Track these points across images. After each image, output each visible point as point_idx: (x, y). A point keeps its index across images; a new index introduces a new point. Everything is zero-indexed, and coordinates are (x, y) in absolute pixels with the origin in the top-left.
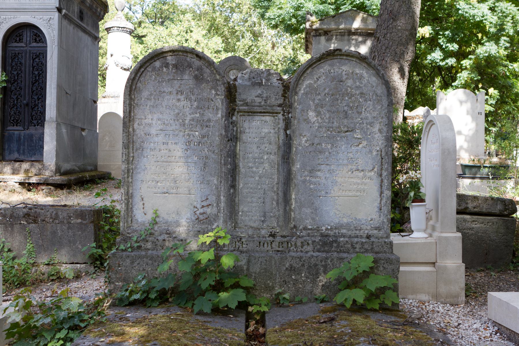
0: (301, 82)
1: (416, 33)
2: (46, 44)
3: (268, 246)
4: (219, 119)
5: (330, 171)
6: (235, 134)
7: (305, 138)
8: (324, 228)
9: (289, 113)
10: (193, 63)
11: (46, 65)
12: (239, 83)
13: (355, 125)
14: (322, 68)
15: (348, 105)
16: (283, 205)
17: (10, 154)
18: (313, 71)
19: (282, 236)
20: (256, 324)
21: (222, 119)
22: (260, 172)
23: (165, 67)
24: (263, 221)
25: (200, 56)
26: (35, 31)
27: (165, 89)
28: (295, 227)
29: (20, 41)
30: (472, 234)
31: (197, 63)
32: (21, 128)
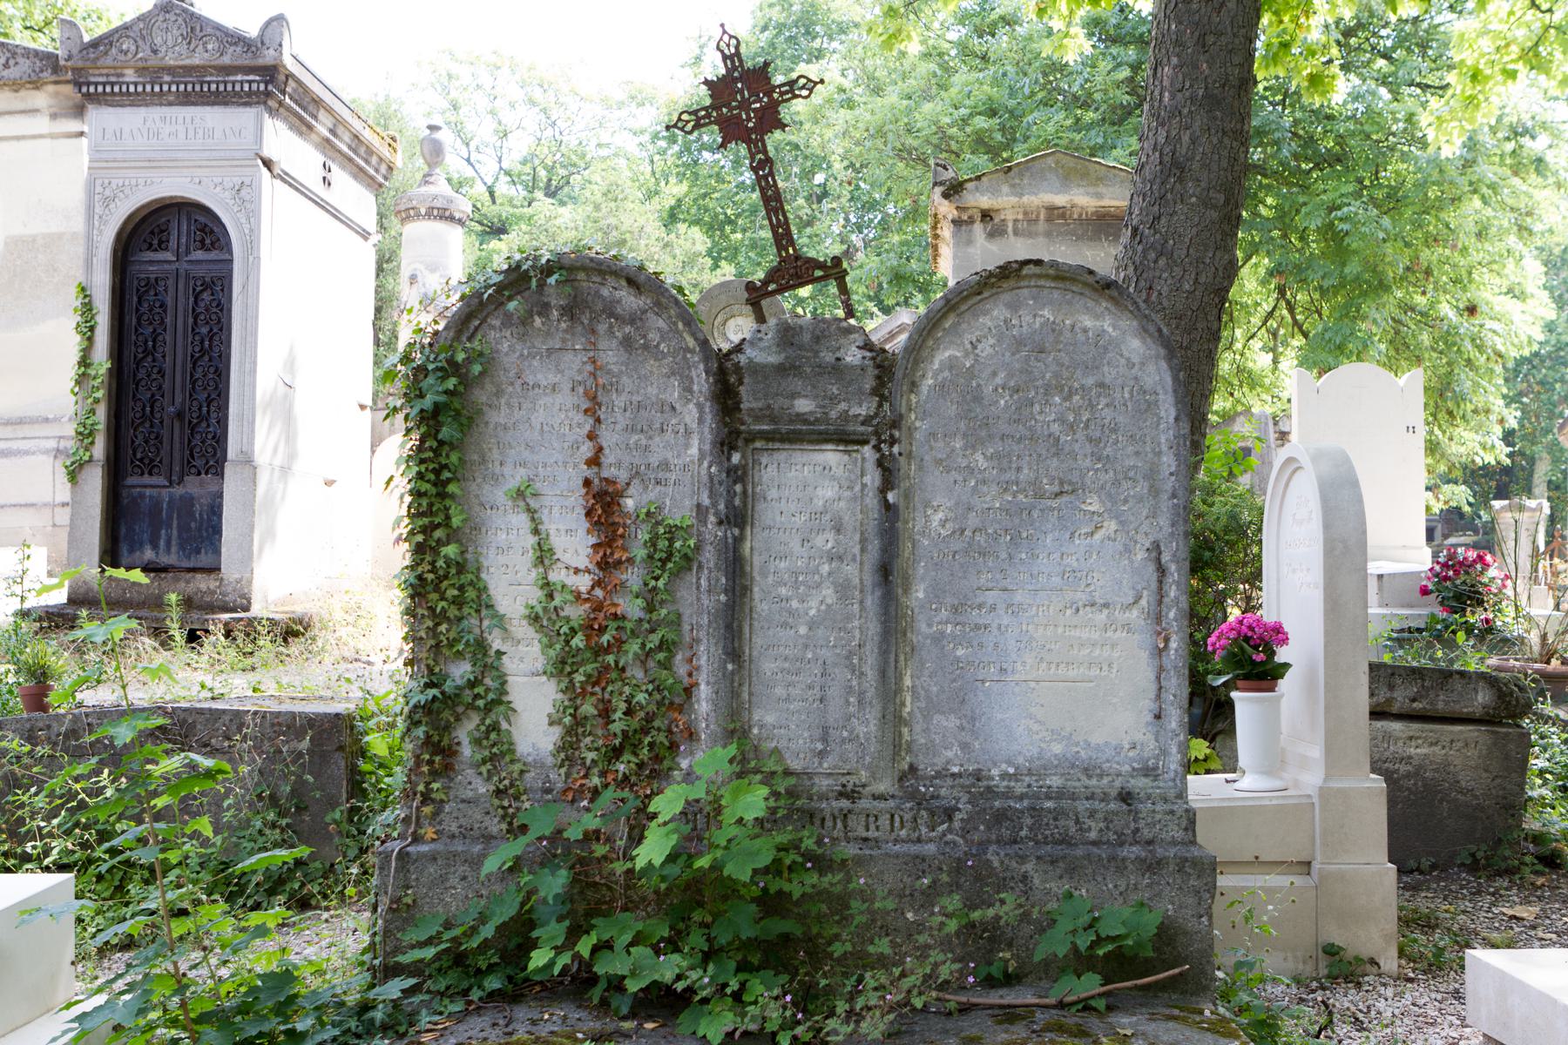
0: (925, 353)
2: (231, 254)
6: (737, 502)
7: (940, 515)
8: (995, 772)
9: (893, 441)
10: (619, 302)
11: (230, 310)
13: (1082, 476)
15: (1061, 420)
16: (878, 707)
17: (131, 551)
18: (959, 323)
19: (875, 797)
21: (701, 460)
22: (812, 612)
23: (540, 314)
24: (822, 754)
25: (638, 280)
26: (202, 219)
27: (539, 376)
28: (913, 769)
29: (162, 245)
30: (1408, 776)
31: (629, 300)
32: (162, 481)
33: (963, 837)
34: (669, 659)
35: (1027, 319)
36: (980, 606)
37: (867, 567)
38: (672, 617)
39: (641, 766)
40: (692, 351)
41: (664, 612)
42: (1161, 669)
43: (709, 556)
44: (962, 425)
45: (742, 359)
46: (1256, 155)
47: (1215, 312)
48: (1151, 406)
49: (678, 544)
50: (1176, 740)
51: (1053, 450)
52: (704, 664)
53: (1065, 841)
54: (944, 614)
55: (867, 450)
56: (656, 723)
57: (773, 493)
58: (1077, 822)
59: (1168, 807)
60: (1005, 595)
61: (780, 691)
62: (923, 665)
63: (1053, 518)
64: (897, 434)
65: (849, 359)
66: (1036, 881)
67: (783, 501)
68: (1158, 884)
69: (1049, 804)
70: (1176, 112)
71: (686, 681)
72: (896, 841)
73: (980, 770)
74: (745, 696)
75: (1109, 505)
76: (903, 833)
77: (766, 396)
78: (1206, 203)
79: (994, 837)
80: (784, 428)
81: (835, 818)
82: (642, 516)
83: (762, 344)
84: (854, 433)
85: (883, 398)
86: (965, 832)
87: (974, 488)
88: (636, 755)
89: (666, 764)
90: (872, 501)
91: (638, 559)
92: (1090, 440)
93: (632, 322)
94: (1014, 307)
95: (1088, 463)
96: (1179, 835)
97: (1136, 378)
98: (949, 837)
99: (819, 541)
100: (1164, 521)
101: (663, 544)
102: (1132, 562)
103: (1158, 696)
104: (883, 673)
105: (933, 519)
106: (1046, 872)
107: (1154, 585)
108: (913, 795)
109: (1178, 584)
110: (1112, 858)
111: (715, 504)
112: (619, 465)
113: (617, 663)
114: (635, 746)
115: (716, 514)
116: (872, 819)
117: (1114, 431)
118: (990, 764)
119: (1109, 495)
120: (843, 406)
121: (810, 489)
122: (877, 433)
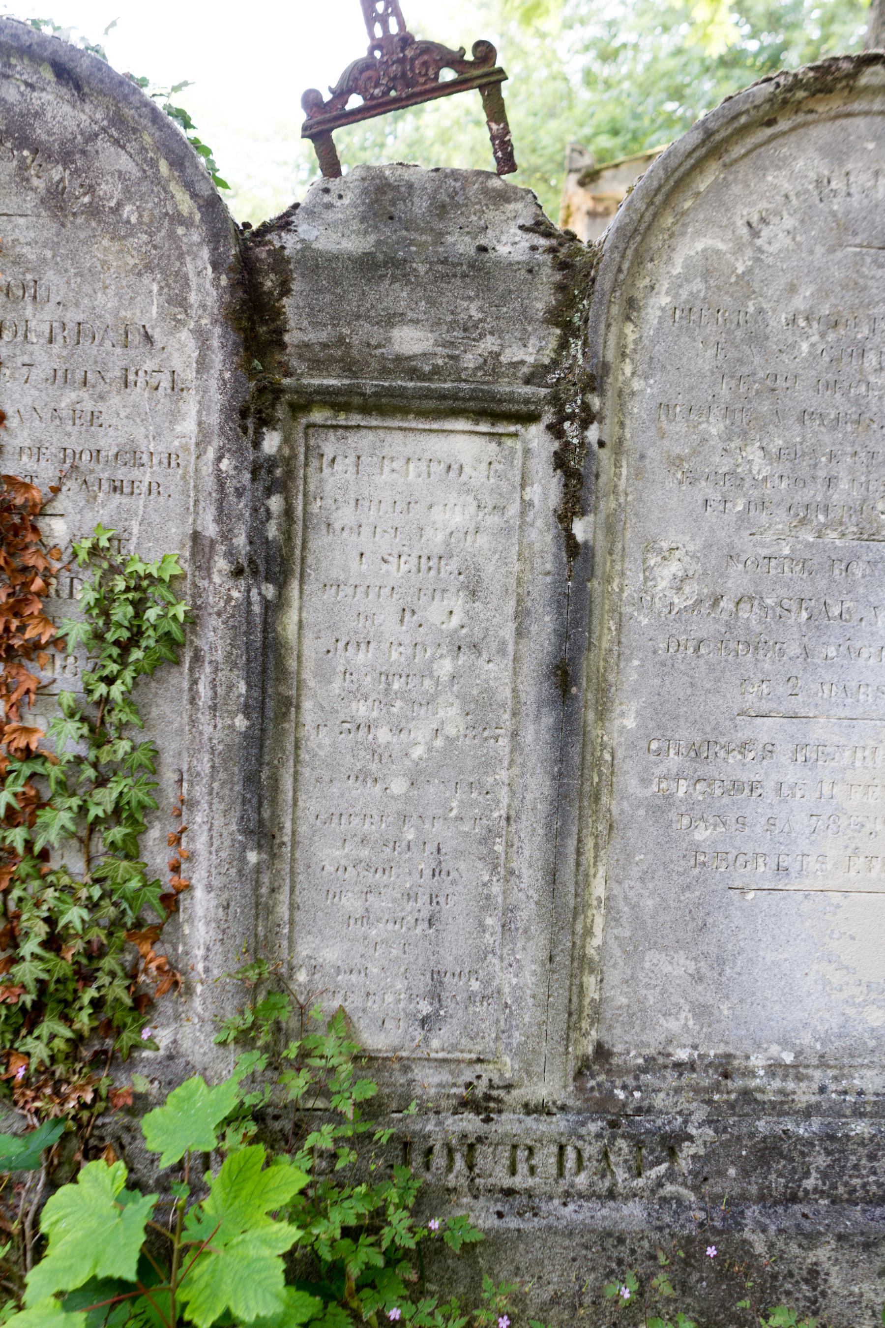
0: (656, 242)
3: (450, 1168)
4: (185, 448)
5: (807, 754)
6: (272, 531)
8: (758, 1061)
9: (587, 418)
12: (306, 246)
14: (780, 164)
18: (726, 184)
19: (529, 1109)
20: (411, 1216)
21: (201, 444)
22: (418, 752)
28: (602, 1052)
31: (61, 114)
33: (695, 1189)
34: (138, 830)
35: (862, 179)
36: (744, 747)
38: (140, 756)
39: (77, 1041)
40: (186, 222)
41: (124, 746)
43: (214, 638)
44: (724, 391)
45: (290, 242)
49: (152, 614)
52: (203, 848)
56: (108, 963)
57: (345, 516)
60: (792, 726)
61: (351, 903)
64: (595, 402)
65: (503, 250)
66: (835, 1281)
67: (366, 531)
69: (861, 1128)
71: (168, 881)
72: (567, 1196)
73: (729, 1056)
74: (283, 911)
76: (582, 1180)
77: (335, 320)
79: (754, 1189)
80: (369, 385)
81: (450, 1152)
82: (83, 555)
83: (330, 216)
84: (511, 398)
85: (569, 331)
86: (699, 1180)
87: (743, 518)
88: (67, 1019)
89: (127, 1038)
90: (542, 536)
91: (71, 641)
93: (66, 158)
94: (837, 154)
98: (670, 1189)
101: (122, 612)
105: (660, 571)
106: (854, 1264)
108: (602, 1106)
111: (226, 536)
112: (38, 451)
113: (29, 845)
114: (67, 1004)
115: (230, 554)
116: (522, 1154)
120: (489, 344)
121: (419, 509)
122: (556, 400)
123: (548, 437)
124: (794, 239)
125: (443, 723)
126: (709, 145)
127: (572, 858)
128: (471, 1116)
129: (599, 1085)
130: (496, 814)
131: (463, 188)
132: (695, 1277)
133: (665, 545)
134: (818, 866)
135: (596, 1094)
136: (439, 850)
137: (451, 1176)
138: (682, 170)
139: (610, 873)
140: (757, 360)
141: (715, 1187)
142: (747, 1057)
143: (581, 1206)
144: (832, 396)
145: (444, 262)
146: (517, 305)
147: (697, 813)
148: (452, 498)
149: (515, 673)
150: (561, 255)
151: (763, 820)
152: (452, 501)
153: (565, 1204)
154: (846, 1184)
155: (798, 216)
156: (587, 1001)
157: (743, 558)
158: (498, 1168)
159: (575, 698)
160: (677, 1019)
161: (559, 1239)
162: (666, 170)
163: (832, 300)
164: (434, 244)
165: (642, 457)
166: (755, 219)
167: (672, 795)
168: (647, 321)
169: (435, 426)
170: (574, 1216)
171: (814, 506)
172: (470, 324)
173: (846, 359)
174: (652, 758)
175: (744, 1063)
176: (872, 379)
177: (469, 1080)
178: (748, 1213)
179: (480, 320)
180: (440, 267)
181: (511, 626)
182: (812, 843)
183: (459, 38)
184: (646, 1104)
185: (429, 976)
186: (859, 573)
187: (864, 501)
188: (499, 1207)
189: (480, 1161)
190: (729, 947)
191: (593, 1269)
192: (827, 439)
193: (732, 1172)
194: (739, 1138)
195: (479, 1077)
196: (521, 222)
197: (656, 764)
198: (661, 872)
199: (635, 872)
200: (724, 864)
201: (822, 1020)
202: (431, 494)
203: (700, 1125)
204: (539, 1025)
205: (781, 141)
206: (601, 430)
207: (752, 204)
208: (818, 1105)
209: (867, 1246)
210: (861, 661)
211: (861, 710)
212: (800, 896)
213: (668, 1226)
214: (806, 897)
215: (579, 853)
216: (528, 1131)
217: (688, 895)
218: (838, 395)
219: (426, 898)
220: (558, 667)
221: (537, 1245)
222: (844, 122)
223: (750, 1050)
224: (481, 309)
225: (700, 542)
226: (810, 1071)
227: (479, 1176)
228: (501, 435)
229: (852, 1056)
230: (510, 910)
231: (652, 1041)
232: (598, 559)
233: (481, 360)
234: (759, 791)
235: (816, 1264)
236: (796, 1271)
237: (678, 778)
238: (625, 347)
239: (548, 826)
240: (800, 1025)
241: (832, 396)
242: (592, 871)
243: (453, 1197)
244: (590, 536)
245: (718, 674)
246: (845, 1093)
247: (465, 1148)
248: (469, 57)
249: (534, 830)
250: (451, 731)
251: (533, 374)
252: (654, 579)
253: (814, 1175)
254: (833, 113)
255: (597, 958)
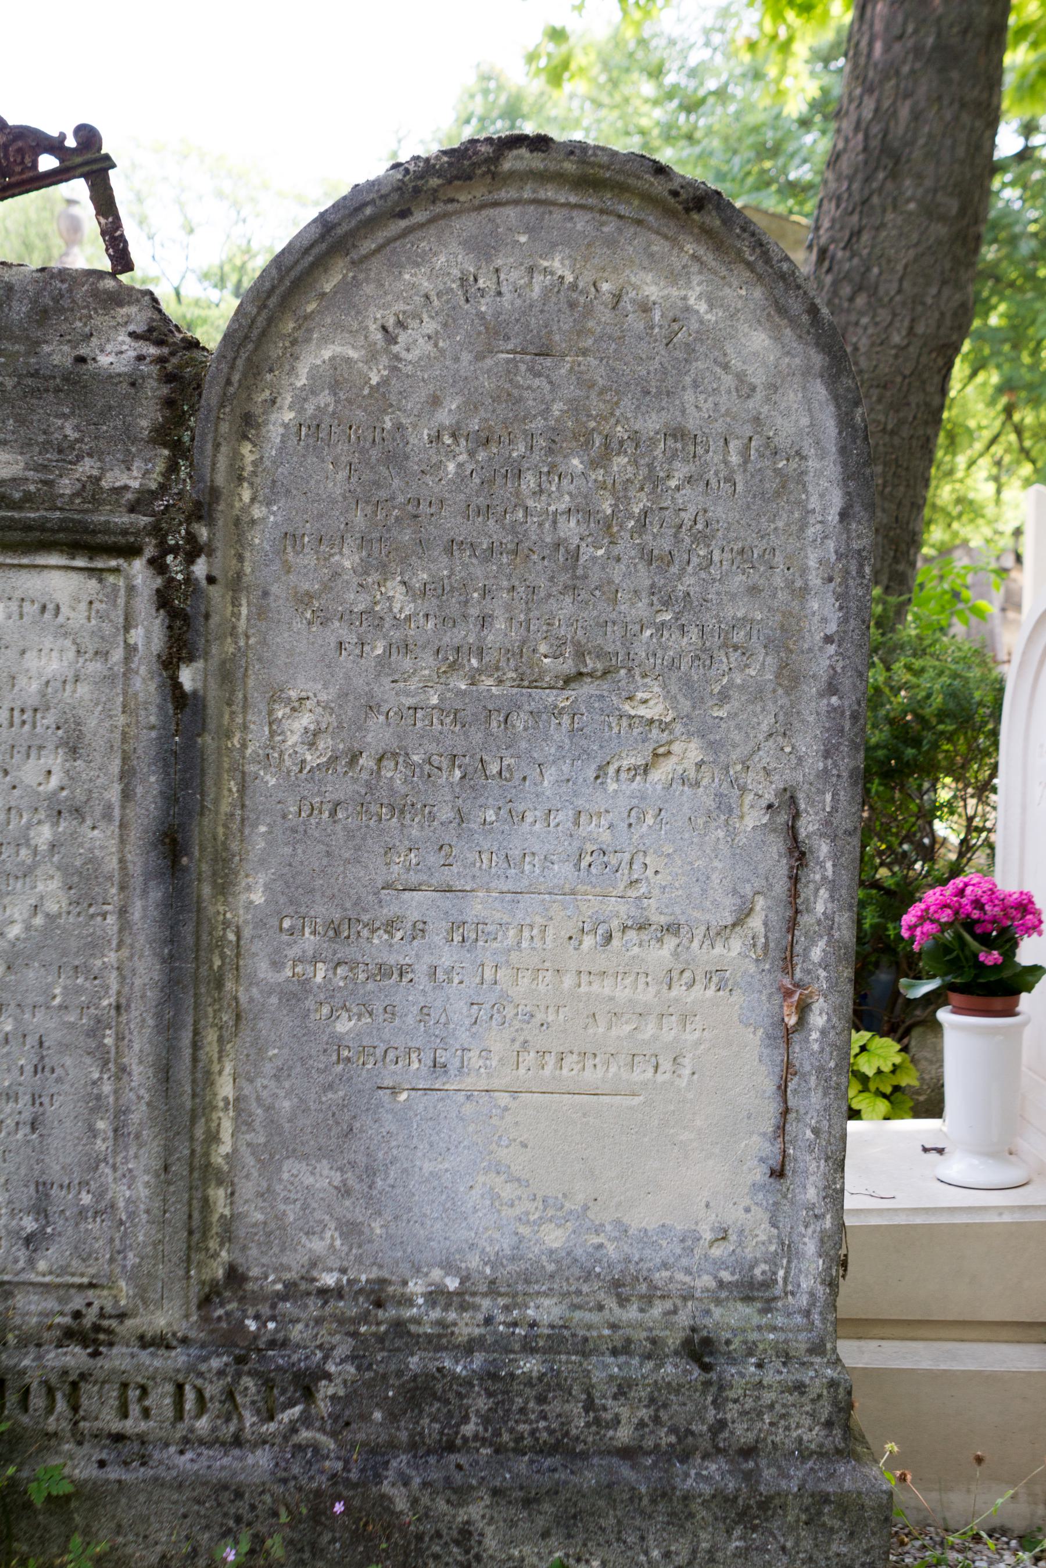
0: (275, 350)
1: (978, 240)
3: (50, 1409)
7: (305, 720)
8: (416, 1287)
9: (193, 551)
13: (628, 639)
15: (585, 511)
18: (356, 283)
19: (145, 1342)
22: (14, 931)
28: (235, 1276)
33: (334, 1434)
35: (514, 276)
36: (390, 926)
37: (134, 834)
42: (788, 1070)
44: (359, 518)
46: (990, 253)
47: (937, 379)
48: (789, 485)
50: (815, 1227)
51: (564, 578)
53: (562, 1447)
54: (309, 941)
55: (138, 567)
58: (589, 1405)
59: (791, 1375)
60: (446, 902)
62: (261, 1051)
63: (559, 732)
64: (203, 533)
65: (104, 360)
66: (491, 1543)
68: (763, 1550)
69: (530, 1365)
70: (891, 71)
72: (186, 1443)
73: (383, 1282)
75: (685, 705)
76: (203, 1424)
78: (930, 211)
79: (403, 1436)
81: (50, 1392)
85: (179, 451)
86: (339, 1425)
87: (383, 663)
90: (145, 685)
92: (649, 558)
94: (483, 249)
95: (641, 609)
96: (813, 1435)
97: (757, 420)
98: (305, 1435)
99: (29, 773)
100: (808, 743)
102: (732, 833)
103: (781, 1129)
104: (165, 1074)
106: (513, 1524)
107: (781, 886)
109: (833, 887)
110: (662, 1494)
116: (133, 1394)
117: (703, 538)
118: (404, 1269)
119: (687, 683)
120: (88, 467)
122: (157, 531)
123: (150, 572)
124: (436, 345)
125: (42, 898)
126: (329, 240)
127: (187, 1052)
128: (77, 1349)
129: (228, 1314)
130: (105, 1003)
131: (70, 290)
132: (326, 1537)
133: (293, 694)
134: (481, 1063)
135: (224, 1325)
136: (41, 1044)
137: (52, 1419)
138: (299, 268)
139: (240, 1070)
140: (396, 483)
141: (361, 1434)
142: (405, 1283)
143: (199, 1455)
144: (484, 523)
145: (35, 374)
146: (119, 423)
147: (338, 1001)
148: (48, 642)
149: (122, 841)
150: (169, 367)
151: (415, 1010)
152: (48, 645)
153: (182, 1452)
154: (511, 1431)
155: (440, 319)
156: (215, 1217)
157: (384, 708)
158: (106, 1410)
159: (185, 870)
160: (322, 1239)
161: (166, 1492)
162: (279, 269)
163: (482, 413)
164: (28, 354)
165: (266, 594)
166: (391, 322)
167: (308, 980)
168: (269, 440)
169: (25, 561)
170: (189, 1466)
171: (465, 649)
172: (65, 445)
173: (499, 481)
174: (285, 937)
175: (400, 1290)
176: (530, 503)
177: (77, 1307)
178: (394, 1464)
179: (77, 440)
180: (29, 381)
181: (116, 788)
182: (473, 1036)
183: (57, 122)
184: (280, 1336)
185: (32, 1188)
186: (520, 726)
187: (524, 642)
188: (104, 1456)
189: (84, 1402)
190: (380, 1155)
191: (207, 1527)
192: (479, 572)
193: (378, 1415)
194: (384, 1377)
195: (89, 1305)
196: (132, 328)
197: (289, 945)
198: (298, 1069)
199: (268, 1068)
200: (372, 1060)
201: (491, 1240)
202: (24, 638)
203: (342, 1361)
204: (155, 1245)
205: (419, 234)
206: (210, 564)
207: (386, 306)
208: (482, 1338)
209: (527, 1503)
210: (526, 826)
211: (526, 882)
212: (461, 1097)
213: (295, 1478)
214: (468, 1097)
215: (196, 1046)
216: (138, 1368)
217: (330, 1095)
218: (491, 522)
219: (28, 1098)
220: (165, 834)
221: (142, 1498)
222: (491, 212)
223: (408, 1274)
224: (77, 428)
225: (333, 691)
226: (477, 1300)
227: (84, 1419)
228: (102, 570)
229: (527, 1282)
230: (120, 1113)
231: (294, 1265)
232: (212, 710)
233: (79, 486)
234: (410, 976)
235: (468, 1522)
236: (445, 1532)
237: (315, 960)
238: (243, 469)
239: (159, 1016)
240: (465, 1246)
241: (484, 523)
242: (216, 1068)
243: (53, 1442)
244: (199, 685)
245: (358, 841)
246: (515, 1324)
247: (67, 1387)
248: (71, 143)
249: (143, 1020)
250: (52, 907)
251: (138, 501)
252: (282, 733)
253: (473, 1419)
254: (477, 202)
255: (226, 1168)
